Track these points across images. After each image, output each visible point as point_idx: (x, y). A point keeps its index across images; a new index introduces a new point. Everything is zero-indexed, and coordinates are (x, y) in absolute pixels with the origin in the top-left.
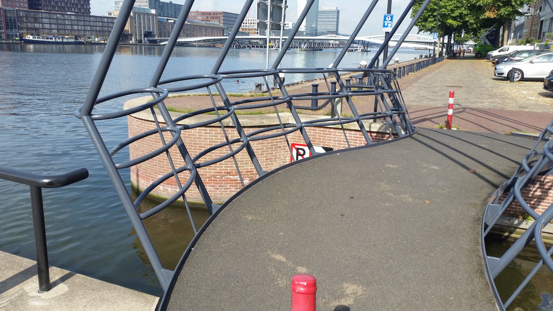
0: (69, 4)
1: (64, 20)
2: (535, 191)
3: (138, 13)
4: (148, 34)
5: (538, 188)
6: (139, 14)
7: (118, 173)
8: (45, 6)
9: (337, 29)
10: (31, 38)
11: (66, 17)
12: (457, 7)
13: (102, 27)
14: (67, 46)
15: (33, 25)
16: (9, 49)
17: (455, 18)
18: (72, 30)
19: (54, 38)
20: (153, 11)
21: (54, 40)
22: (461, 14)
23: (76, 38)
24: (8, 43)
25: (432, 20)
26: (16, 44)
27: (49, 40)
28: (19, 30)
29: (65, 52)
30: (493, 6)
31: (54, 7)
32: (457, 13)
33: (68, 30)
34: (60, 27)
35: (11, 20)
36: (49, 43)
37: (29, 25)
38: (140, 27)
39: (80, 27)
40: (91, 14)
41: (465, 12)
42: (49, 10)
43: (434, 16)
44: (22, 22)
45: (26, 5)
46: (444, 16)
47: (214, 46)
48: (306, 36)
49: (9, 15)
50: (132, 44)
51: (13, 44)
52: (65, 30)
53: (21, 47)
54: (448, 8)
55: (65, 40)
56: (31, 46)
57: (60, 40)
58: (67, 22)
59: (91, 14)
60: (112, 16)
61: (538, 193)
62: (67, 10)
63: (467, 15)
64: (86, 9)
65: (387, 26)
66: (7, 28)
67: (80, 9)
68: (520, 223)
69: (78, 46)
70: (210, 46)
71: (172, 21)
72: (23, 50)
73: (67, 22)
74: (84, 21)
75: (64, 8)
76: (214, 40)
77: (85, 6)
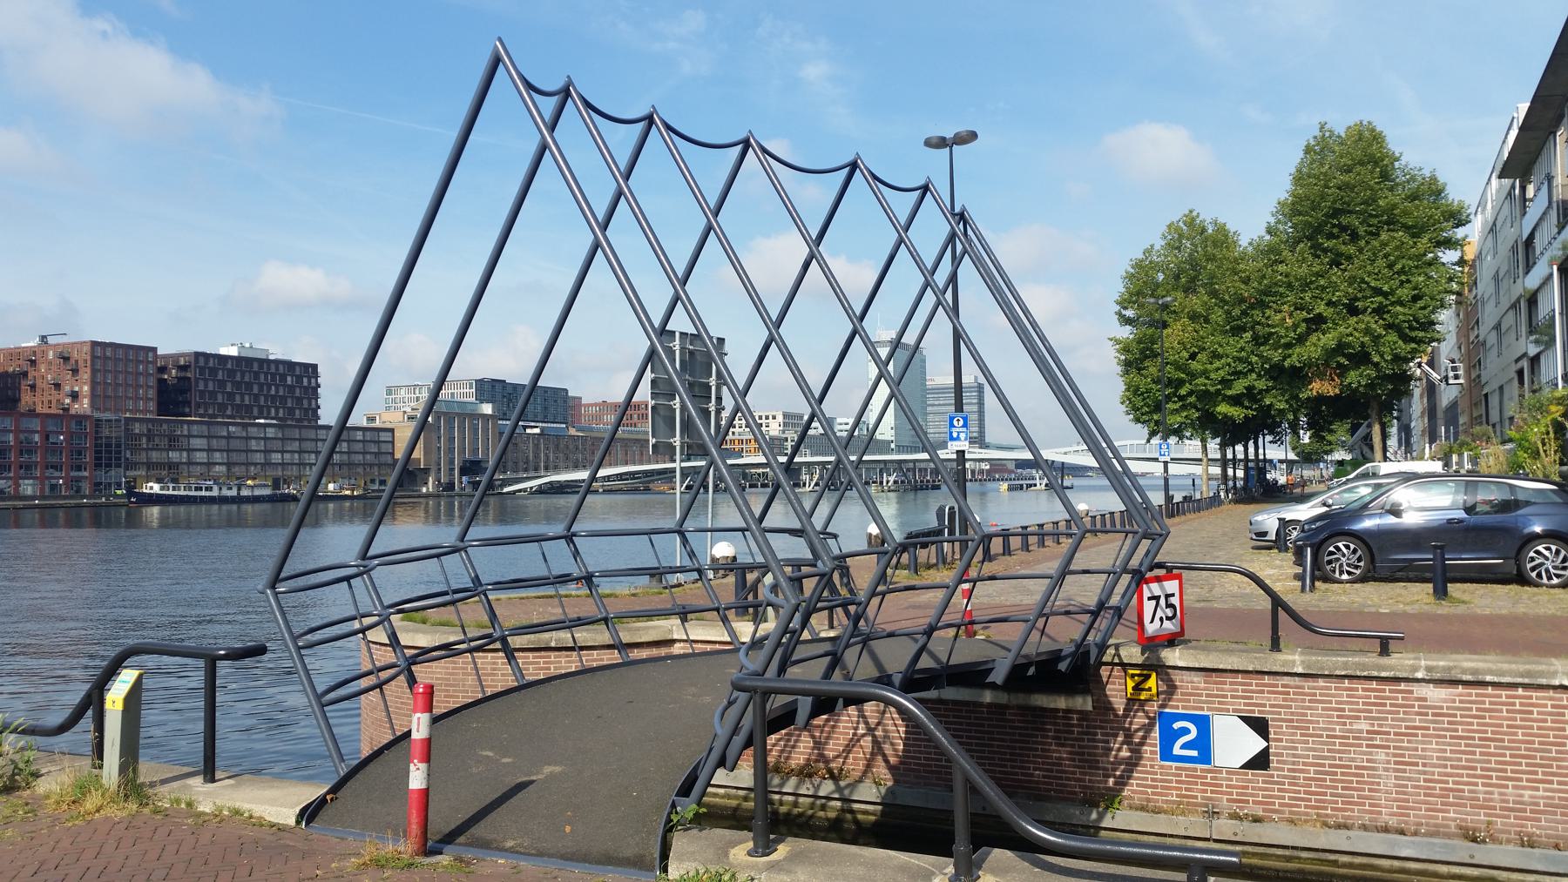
0: (262, 377)
1: (248, 438)
2: (1119, 750)
3: (445, 414)
4: (471, 468)
5: (1123, 743)
6: (450, 417)
7: (326, 719)
8: (198, 406)
9: (982, 432)
10: (156, 488)
11: (253, 431)
12: (1238, 374)
13: (349, 453)
14: (248, 508)
15: (164, 454)
16: (97, 523)
17: (1236, 401)
18: (267, 464)
19: (216, 488)
20: (487, 409)
21: (215, 493)
22: (1250, 389)
23: (276, 485)
24: (94, 506)
25: (1176, 406)
26: (116, 505)
27: (203, 493)
28: (127, 469)
29: (188, 525)
30: (1327, 364)
31: (222, 407)
32: (1239, 387)
33: (256, 464)
34: (235, 457)
35: (108, 445)
36: (203, 500)
37: (155, 456)
38: (451, 450)
39: (287, 456)
40: (320, 422)
41: (1261, 385)
42: (211, 416)
43: (1181, 398)
44: (136, 449)
45: (152, 406)
46: (1205, 396)
47: (647, 490)
48: (899, 452)
49: (106, 432)
50: (427, 496)
51: (107, 506)
52: (248, 464)
53: (128, 514)
54: (1213, 376)
55: (245, 492)
56: (155, 511)
57: (234, 492)
58: (253, 444)
59: (320, 422)
60: (377, 424)
61: (1125, 753)
62: (256, 411)
63: (1267, 391)
64: (306, 410)
65: (958, 438)
66: (98, 466)
67: (291, 411)
68: (1101, 817)
69: (279, 505)
70: (635, 490)
71: (537, 431)
72: (133, 521)
73: (253, 444)
74: (300, 440)
75: (249, 408)
76: (646, 473)
77: (305, 402)
